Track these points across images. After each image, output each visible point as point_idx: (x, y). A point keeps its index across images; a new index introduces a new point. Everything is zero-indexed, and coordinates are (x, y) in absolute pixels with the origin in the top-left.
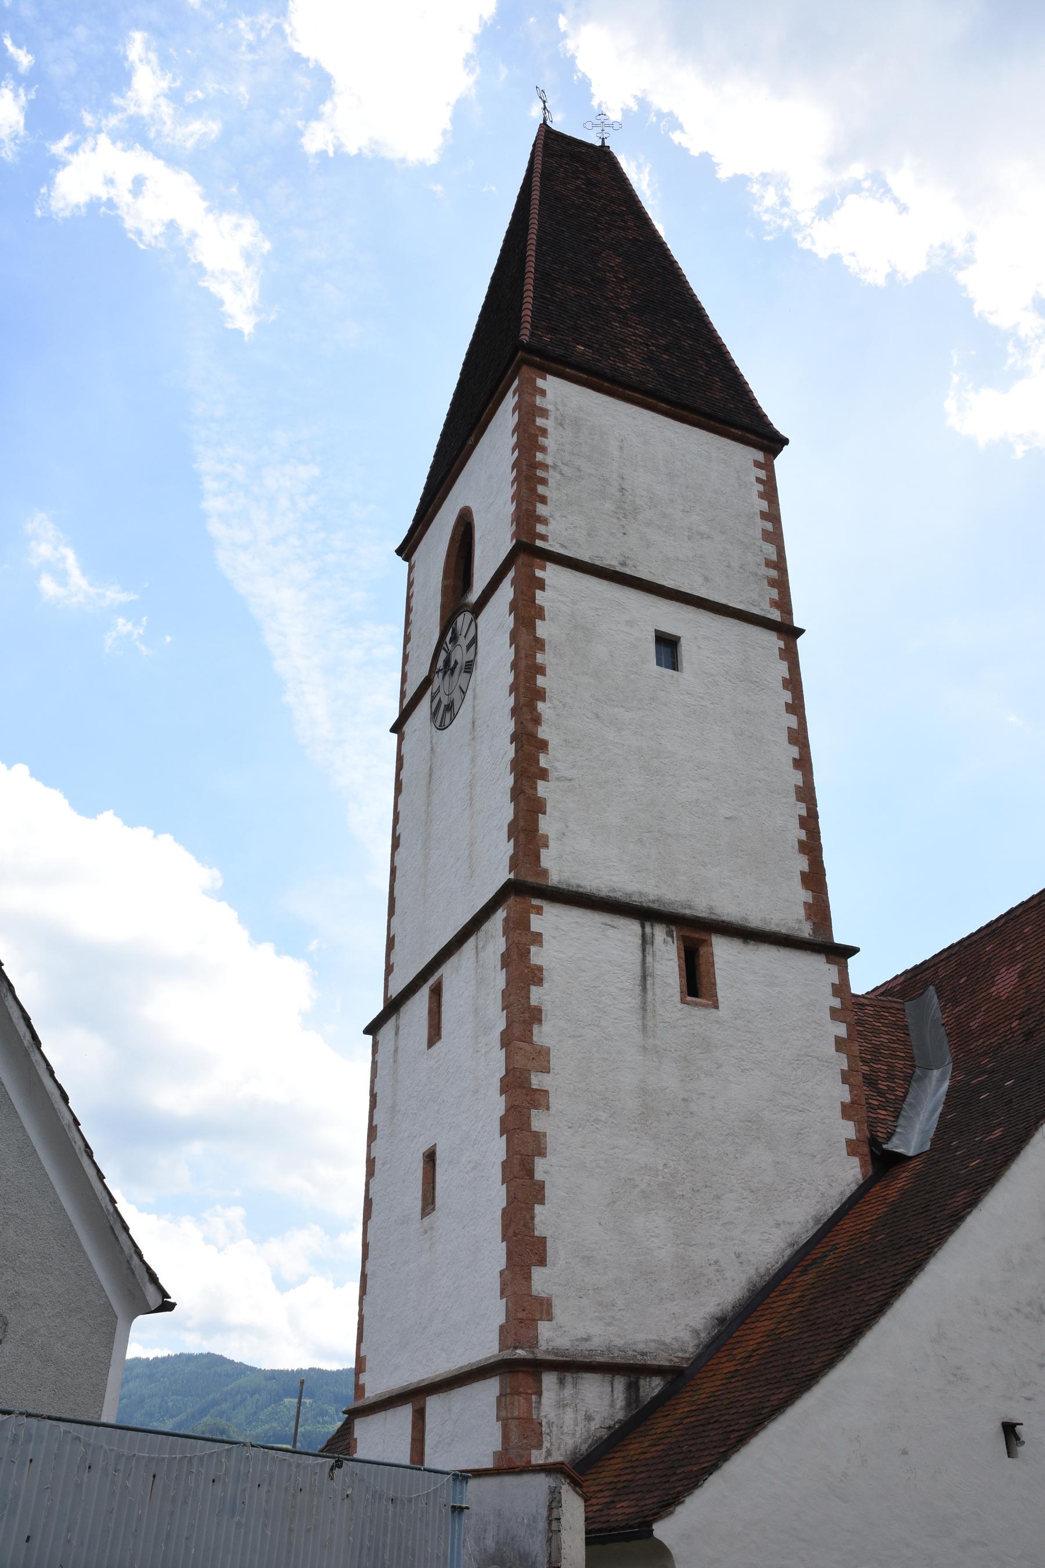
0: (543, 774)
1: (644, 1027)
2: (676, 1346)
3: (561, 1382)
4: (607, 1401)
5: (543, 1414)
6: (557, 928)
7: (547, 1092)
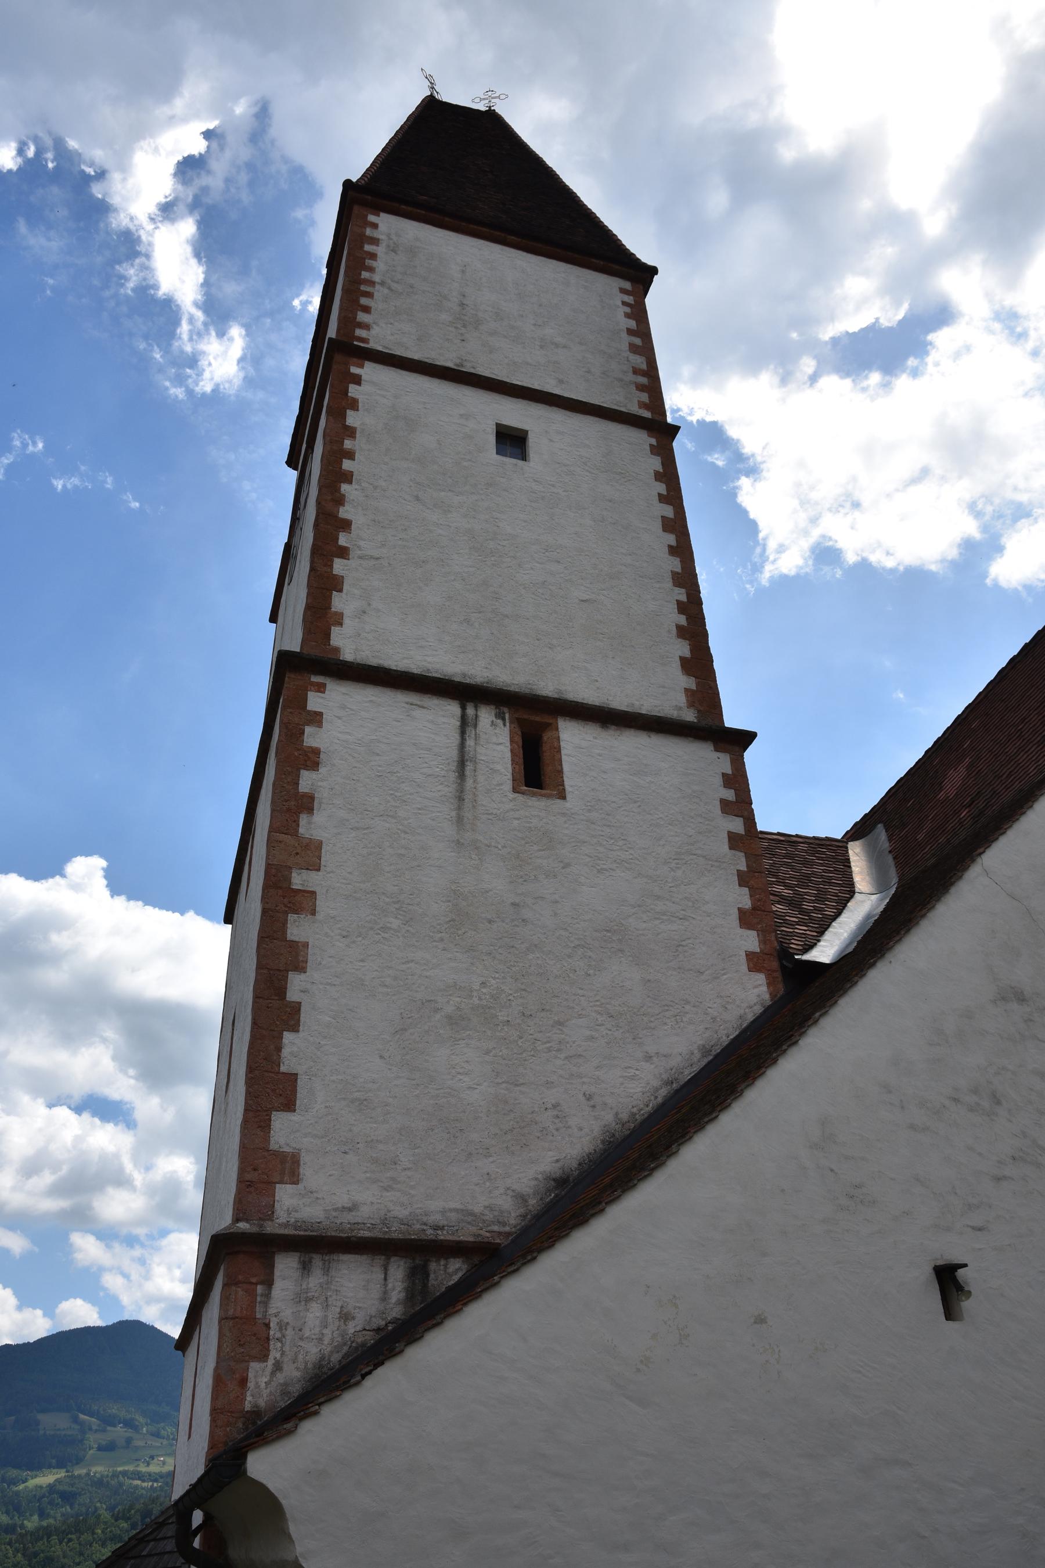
0: (343, 553)
1: (460, 820)
2: (489, 1216)
3: (306, 1267)
4: (376, 1291)
5: (272, 1311)
6: (343, 707)
7: (314, 893)
